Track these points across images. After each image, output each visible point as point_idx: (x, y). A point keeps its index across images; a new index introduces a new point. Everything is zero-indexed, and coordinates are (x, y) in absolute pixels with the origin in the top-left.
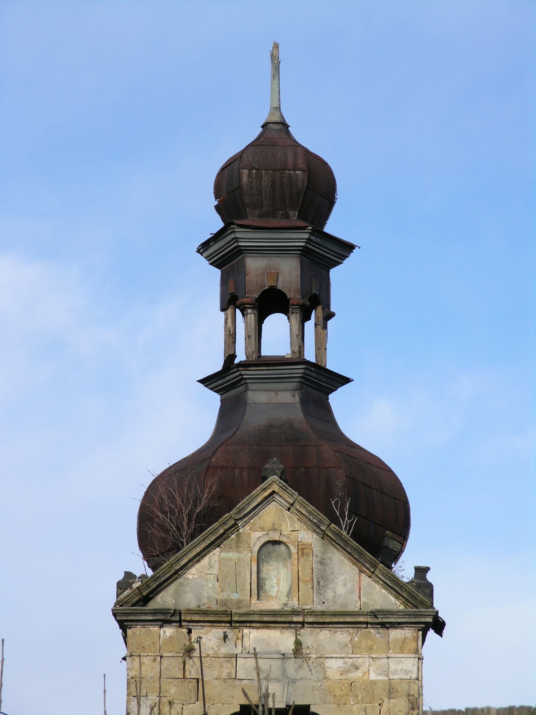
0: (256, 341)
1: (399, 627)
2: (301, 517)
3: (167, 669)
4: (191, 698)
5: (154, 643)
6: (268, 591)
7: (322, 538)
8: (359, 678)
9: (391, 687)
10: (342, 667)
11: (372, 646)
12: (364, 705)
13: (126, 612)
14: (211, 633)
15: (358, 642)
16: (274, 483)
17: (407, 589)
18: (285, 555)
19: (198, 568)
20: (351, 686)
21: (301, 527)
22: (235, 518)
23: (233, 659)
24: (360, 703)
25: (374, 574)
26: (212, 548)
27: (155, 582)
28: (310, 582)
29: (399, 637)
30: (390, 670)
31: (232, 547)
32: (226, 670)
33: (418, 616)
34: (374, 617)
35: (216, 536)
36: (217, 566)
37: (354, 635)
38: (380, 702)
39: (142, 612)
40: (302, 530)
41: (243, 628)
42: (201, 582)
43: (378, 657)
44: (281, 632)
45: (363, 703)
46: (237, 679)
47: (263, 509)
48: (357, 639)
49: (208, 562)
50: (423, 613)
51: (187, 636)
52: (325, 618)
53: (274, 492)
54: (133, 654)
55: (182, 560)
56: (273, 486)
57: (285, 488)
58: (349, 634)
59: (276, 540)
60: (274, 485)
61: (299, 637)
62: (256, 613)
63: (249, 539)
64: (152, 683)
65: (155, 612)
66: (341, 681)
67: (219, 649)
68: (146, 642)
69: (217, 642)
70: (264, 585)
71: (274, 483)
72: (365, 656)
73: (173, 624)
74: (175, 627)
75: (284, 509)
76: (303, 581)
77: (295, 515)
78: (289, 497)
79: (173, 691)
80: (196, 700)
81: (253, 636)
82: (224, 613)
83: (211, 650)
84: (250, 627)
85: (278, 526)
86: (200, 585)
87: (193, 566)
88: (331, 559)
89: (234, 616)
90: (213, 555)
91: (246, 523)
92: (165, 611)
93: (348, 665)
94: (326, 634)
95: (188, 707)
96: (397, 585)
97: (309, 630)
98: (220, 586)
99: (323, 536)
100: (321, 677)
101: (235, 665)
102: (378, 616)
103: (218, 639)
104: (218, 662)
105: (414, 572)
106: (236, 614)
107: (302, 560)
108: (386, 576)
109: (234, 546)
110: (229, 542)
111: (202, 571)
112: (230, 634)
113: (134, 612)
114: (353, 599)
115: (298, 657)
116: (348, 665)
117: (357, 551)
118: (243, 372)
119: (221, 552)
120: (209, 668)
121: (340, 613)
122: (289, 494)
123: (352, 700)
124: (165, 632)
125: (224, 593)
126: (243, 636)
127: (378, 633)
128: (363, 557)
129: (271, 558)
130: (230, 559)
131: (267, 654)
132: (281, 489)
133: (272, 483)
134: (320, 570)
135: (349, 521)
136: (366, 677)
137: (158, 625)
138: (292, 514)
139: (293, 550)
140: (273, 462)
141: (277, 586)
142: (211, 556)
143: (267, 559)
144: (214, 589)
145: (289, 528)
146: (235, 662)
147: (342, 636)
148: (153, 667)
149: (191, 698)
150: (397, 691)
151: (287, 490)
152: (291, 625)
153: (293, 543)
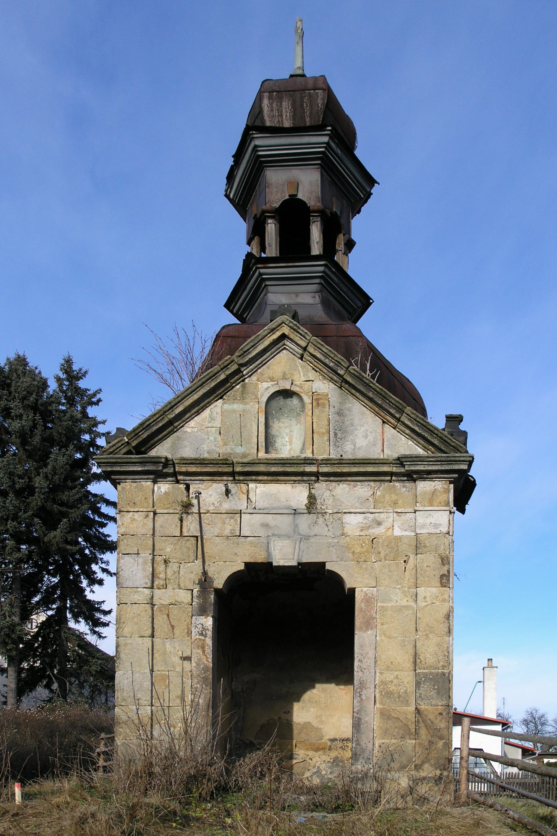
0: (276, 250)
1: (428, 478)
2: (315, 364)
3: (161, 526)
4: (189, 556)
5: (146, 498)
6: (279, 449)
7: (340, 388)
8: (382, 534)
9: (418, 542)
10: (362, 522)
12: (387, 562)
13: (109, 460)
14: (211, 488)
15: (381, 496)
16: (283, 324)
17: (439, 433)
18: (298, 409)
19: (197, 421)
20: (373, 543)
21: (316, 377)
22: (239, 363)
23: (237, 514)
24: (383, 560)
25: (400, 423)
26: (213, 399)
27: (145, 431)
28: (326, 434)
29: (428, 489)
30: (417, 524)
31: (236, 398)
32: (230, 526)
33: (452, 463)
34: (400, 466)
35: (217, 382)
36: (219, 418)
37: (376, 489)
38: (406, 558)
39: (129, 460)
40: (318, 380)
41: (248, 482)
42: (200, 436)
43: (404, 511)
44: (293, 486)
45: (385, 560)
46: (242, 536)
47: (273, 357)
48: (380, 494)
49: (209, 414)
50: (457, 459)
51: (185, 492)
52: (343, 467)
53: (283, 337)
54: (122, 509)
55: (176, 408)
56: (283, 328)
57: (296, 328)
58: (371, 488)
59: (287, 388)
60: (283, 326)
61: (313, 491)
62: (262, 461)
63: (256, 390)
64: (144, 540)
66: (361, 537)
67: (221, 505)
68: (138, 497)
69: (219, 498)
70: (275, 443)
71: (283, 324)
72: (389, 511)
73: (169, 479)
74: (170, 483)
75: (296, 358)
76: (318, 433)
77: (309, 363)
78: (302, 339)
79: (168, 550)
80: (194, 559)
81: (260, 490)
82: (224, 462)
83: (212, 506)
84: (256, 481)
85: (289, 376)
86: (200, 439)
87: (191, 418)
88: (349, 410)
89: (237, 466)
90: (215, 407)
91: (252, 372)
92: (155, 460)
93: (369, 521)
94: (345, 488)
95: (186, 566)
96: (427, 431)
97: (324, 484)
98: (222, 440)
99: (341, 385)
100: (339, 533)
101: (239, 521)
102: (405, 463)
103: (219, 495)
104: (219, 518)
105: (445, 421)
106: (238, 463)
107: (316, 411)
108: (414, 421)
109: (239, 397)
110: (233, 393)
111: (202, 423)
112: (233, 489)
113: (119, 460)
114: (376, 452)
115: (312, 512)
116: (369, 521)
117: (381, 394)
118: (262, 271)
120: (209, 524)
121: (361, 461)
122: (301, 334)
123: (373, 557)
124: (159, 488)
125: (227, 446)
126: (248, 491)
127: (404, 486)
128: (387, 401)
129: (282, 414)
130: (234, 411)
131: (275, 509)
132: (292, 330)
133: (282, 324)
134: (338, 422)
135: (370, 374)
136: (389, 533)
137: (150, 479)
138: (305, 363)
139: (307, 400)
140: (284, 308)
141: (290, 444)
142: (213, 408)
143: (278, 415)
144: (216, 442)
145: (302, 378)
146: (239, 518)
147: (363, 490)
148: (145, 523)
149: (189, 556)
150: (425, 546)
151: (299, 330)
152: (304, 478)
153: (307, 393)
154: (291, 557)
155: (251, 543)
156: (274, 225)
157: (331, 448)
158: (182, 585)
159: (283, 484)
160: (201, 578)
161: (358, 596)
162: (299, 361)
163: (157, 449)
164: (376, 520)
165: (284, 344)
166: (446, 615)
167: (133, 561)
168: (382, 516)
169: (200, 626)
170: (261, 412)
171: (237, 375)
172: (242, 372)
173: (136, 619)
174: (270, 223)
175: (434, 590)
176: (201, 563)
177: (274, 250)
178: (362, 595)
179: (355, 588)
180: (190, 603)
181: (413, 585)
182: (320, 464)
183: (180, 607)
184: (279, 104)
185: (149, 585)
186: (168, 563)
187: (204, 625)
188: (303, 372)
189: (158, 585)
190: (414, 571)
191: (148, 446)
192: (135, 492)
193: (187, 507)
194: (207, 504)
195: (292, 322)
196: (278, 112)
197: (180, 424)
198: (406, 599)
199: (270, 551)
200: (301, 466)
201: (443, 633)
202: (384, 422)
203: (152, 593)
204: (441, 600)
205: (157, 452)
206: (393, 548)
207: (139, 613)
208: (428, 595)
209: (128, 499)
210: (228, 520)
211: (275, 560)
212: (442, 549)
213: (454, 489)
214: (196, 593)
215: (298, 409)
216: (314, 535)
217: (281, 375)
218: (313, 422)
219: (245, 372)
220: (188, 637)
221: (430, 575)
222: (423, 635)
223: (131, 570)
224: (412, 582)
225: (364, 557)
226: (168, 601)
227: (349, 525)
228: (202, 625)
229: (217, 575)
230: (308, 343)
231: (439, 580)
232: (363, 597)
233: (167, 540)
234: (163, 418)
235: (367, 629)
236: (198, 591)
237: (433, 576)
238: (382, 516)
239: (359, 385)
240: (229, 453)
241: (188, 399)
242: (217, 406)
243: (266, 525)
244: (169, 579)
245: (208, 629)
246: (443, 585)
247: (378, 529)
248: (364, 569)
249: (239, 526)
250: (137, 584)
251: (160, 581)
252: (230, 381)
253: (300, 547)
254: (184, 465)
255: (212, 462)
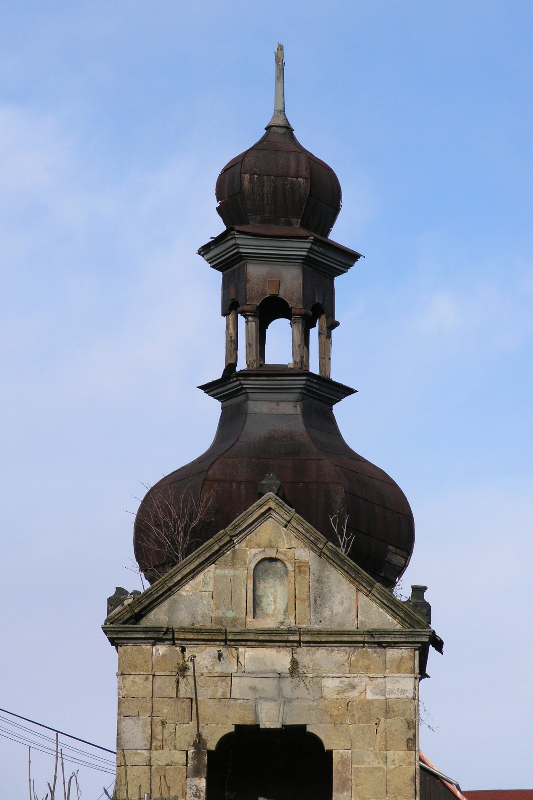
0: (257, 349)
1: (395, 646)
3: (159, 688)
5: (146, 661)
6: (264, 609)
11: (369, 665)
12: (361, 724)
13: (116, 629)
18: (282, 572)
20: (348, 706)
21: (298, 544)
22: (231, 535)
23: (228, 678)
24: (357, 723)
28: (307, 600)
29: (396, 656)
31: (227, 563)
36: (212, 583)
37: (350, 654)
38: (377, 721)
40: (300, 547)
41: (238, 646)
43: (375, 676)
45: (359, 722)
46: (232, 699)
48: (354, 659)
49: (203, 579)
51: (181, 654)
53: (270, 509)
54: (125, 672)
56: (270, 502)
57: (281, 505)
58: (346, 653)
60: (270, 501)
61: (295, 656)
62: (251, 631)
63: (244, 556)
65: (147, 630)
66: (337, 700)
67: (213, 668)
69: (212, 661)
71: (270, 500)
72: (362, 675)
73: (166, 642)
75: (281, 526)
76: (300, 599)
78: (286, 514)
79: (165, 711)
80: (189, 720)
81: (248, 655)
83: (206, 669)
86: (195, 603)
87: (187, 582)
88: (328, 577)
89: (229, 635)
90: (208, 571)
91: (242, 539)
93: (345, 685)
94: (323, 653)
98: (215, 604)
100: (318, 696)
101: (230, 684)
102: (374, 636)
106: (231, 632)
107: (298, 578)
108: (383, 595)
109: (230, 563)
111: (197, 587)
115: (295, 676)
116: (345, 685)
118: (242, 382)
119: (216, 569)
120: (203, 687)
124: (157, 650)
125: (219, 611)
126: (238, 654)
127: (375, 652)
130: (225, 576)
132: (277, 506)
133: (268, 500)
135: (347, 539)
136: (362, 697)
139: (290, 567)
141: (274, 604)
142: (206, 573)
143: (263, 576)
144: (209, 607)
145: (286, 545)
146: (230, 681)
147: (339, 655)
148: (145, 686)
150: (394, 711)
152: (288, 644)
153: (290, 560)
154: (276, 719)
155: (241, 706)
156: (254, 323)
157: (312, 614)
158: (178, 746)
159: (269, 649)
160: (196, 740)
161: (335, 758)
162: (283, 530)
163: (155, 611)
164: (351, 684)
165: (270, 514)
166: (412, 778)
167: (133, 724)
168: (356, 680)
169: (194, 788)
170: (249, 578)
171: (228, 544)
172: (233, 541)
173: (135, 781)
174: (251, 321)
175: (402, 753)
176: (196, 725)
177: (254, 350)
178: (338, 757)
179: (332, 750)
180: (185, 764)
181: (384, 747)
182: (302, 634)
183: (176, 768)
184: (260, 189)
185: (148, 747)
186: (165, 724)
187: (198, 787)
188: (287, 540)
189: (155, 746)
190: (384, 734)
191: (148, 610)
192: (136, 655)
193: (183, 670)
194: (201, 667)
195: (277, 500)
196: (259, 197)
197: (177, 588)
198: (377, 761)
199: (257, 713)
200: (285, 636)
201: (410, 795)
202: (357, 589)
203: (150, 755)
204: (407, 763)
205: (155, 614)
206: (366, 711)
207: (138, 775)
208: (396, 758)
209: (129, 662)
210: (220, 682)
211: (262, 722)
212: (408, 714)
213: (419, 656)
214: (191, 754)
215: (282, 572)
216: (296, 698)
217: (267, 542)
218: (295, 588)
219: (235, 541)
220: (182, 798)
221: (398, 739)
222: (392, 797)
223: (131, 732)
224: (382, 744)
225: (340, 720)
226: (165, 762)
227: (327, 689)
228: (197, 786)
229: (210, 737)
230: (292, 518)
231: (406, 744)
232: (339, 759)
233: (164, 701)
234: (163, 586)
235: (343, 791)
236: (193, 753)
237: (400, 740)
238: (356, 680)
239: (336, 559)
240: (220, 617)
241: (185, 569)
242: (210, 571)
243: (253, 689)
244: (166, 740)
245: (202, 791)
246: (409, 749)
247: (352, 693)
248: (340, 732)
249: (230, 689)
250: (137, 746)
251: (158, 742)
252: (223, 549)
253: (284, 710)
254: (182, 633)
255: (208, 631)
